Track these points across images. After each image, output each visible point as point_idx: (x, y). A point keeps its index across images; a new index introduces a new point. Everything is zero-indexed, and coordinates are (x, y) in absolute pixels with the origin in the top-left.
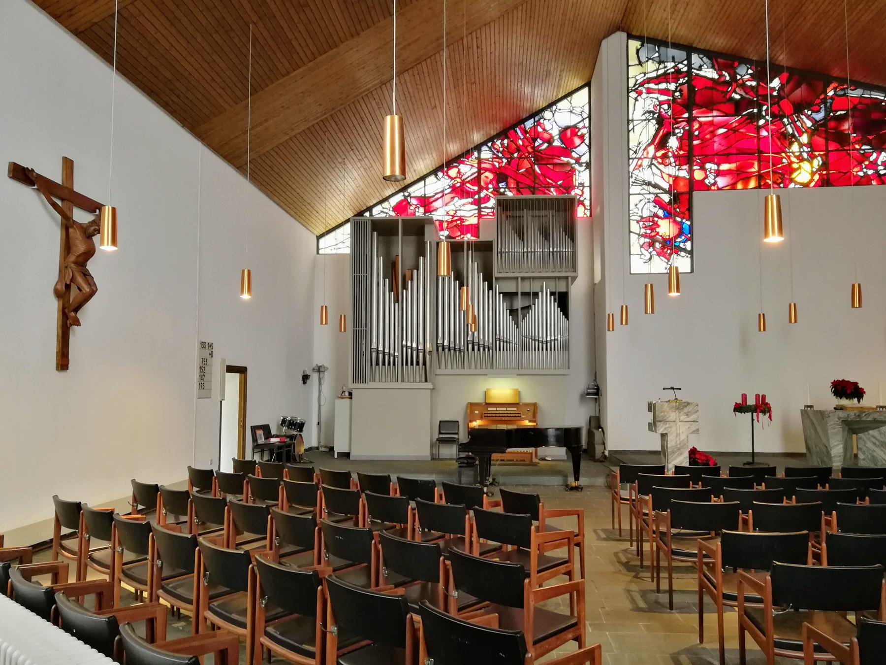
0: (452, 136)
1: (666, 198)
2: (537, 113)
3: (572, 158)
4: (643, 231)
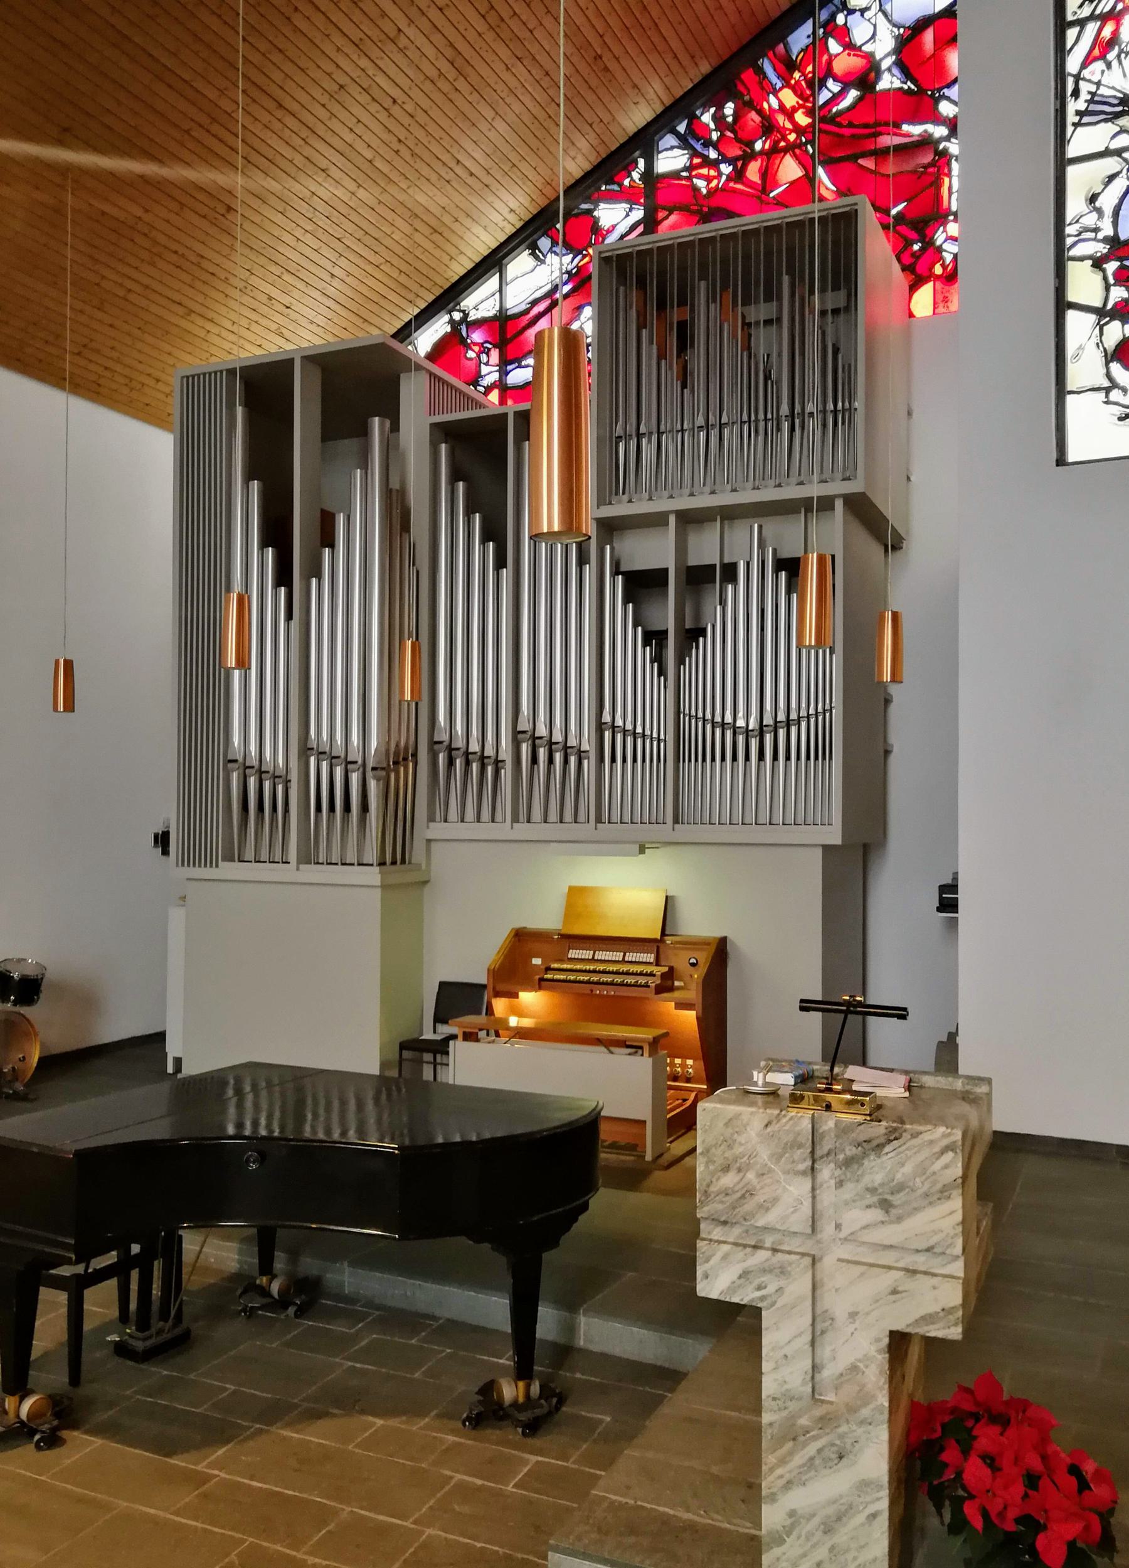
3: (938, 119)
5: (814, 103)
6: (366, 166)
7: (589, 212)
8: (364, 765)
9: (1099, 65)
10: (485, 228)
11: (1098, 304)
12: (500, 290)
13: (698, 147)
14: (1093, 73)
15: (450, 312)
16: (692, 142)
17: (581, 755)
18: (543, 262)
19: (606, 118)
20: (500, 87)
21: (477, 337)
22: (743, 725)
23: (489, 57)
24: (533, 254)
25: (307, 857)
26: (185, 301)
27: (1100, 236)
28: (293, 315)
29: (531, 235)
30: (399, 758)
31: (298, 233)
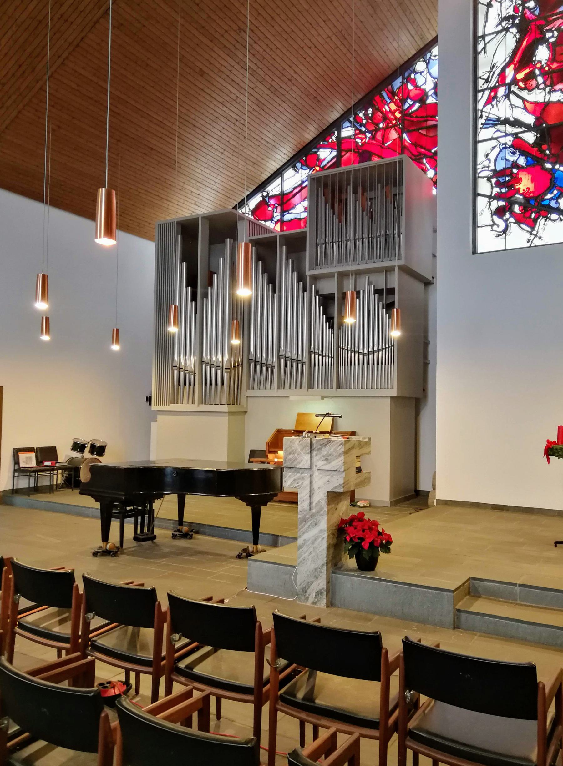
0: (304, 116)
1: (530, 137)
2: (408, 66)
4: (496, 190)
5: (402, 109)
6: (227, 144)
7: (316, 152)
8: (222, 367)
9: (489, 106)
10: (274, 161)
11: (489, 194)
12: (281, 184)
13: (358, 126)
14: (487, 109)
15: (262, 193)
16: (356, 124)
17: (303, 363)
18: (298, 172)
19: (320, 118)
20: (277, 112)
21: (272, 202)
22: (362, 351)
23: (272, 102)
24: (294, 169)
26: (160, 195)
27: (490, 169)
28: (201, 198)
29: (293, 162)
31: (202, 168)
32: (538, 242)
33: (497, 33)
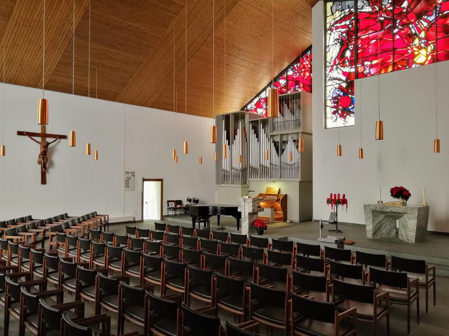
1: (344, 85)
4: (333, 105)
21: (262, 101)
25: (232, 183)
30: (244, 170)
32: (347, 125)
33: (333, 45)
